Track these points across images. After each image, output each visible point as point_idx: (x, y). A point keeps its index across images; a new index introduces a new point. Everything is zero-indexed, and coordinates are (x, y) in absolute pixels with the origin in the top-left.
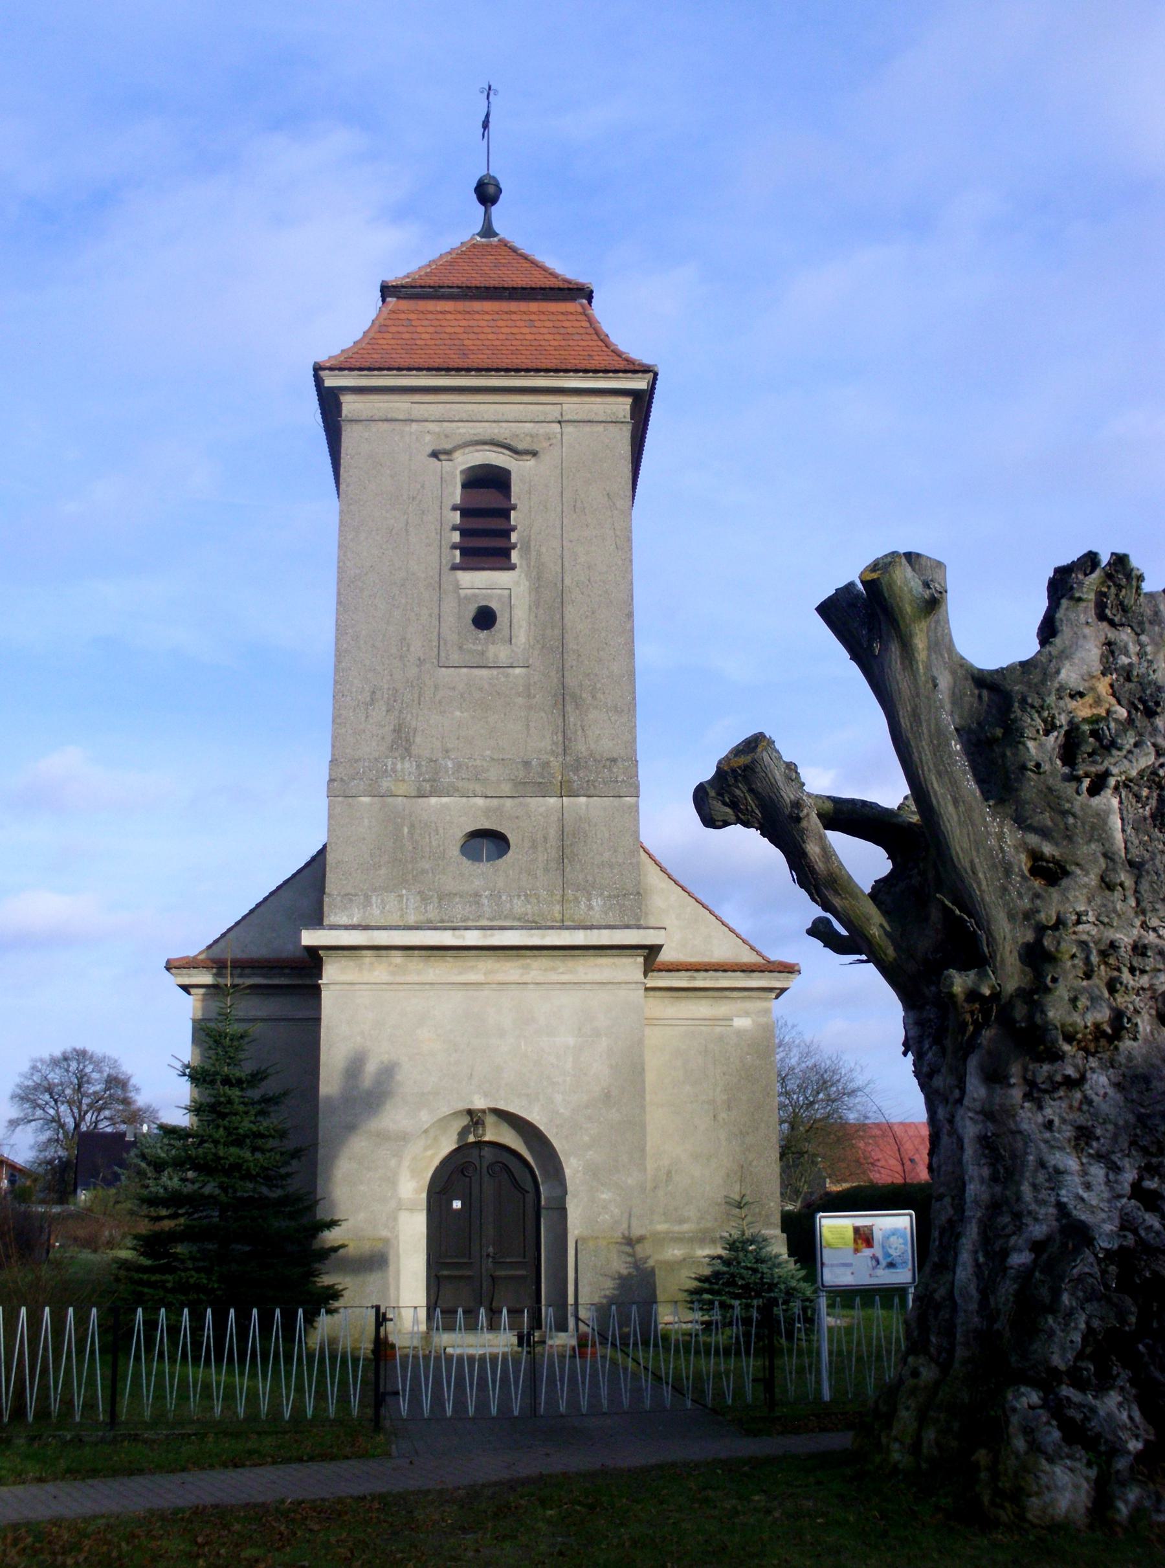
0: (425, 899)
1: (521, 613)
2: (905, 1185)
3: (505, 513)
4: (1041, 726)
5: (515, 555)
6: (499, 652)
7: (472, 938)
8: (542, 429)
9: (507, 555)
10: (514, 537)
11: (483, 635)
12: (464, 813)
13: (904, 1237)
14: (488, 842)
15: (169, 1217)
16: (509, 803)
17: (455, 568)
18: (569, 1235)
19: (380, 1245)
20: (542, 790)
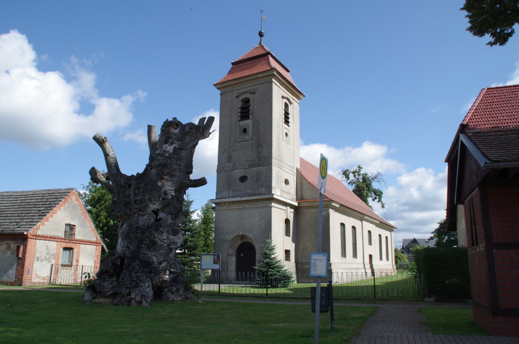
0: (233, 191)
1: (251, 128)
2: (447, 210)
3: (248, 107)
4: (149, 291)
5: (250, 117)
6: (247, 137)
7: (238, 199)
8: (256, 87)
9: (248, 116)
10: (250, 112)
11: (244, 134)
12: (238, 173)
13: (19, 281)
14: (243, 179)
15: (193, 261)
16: (248, 170)
17: (239, 121)
18: (292, 237)
19: (239, 242)
20: (254, 166)
